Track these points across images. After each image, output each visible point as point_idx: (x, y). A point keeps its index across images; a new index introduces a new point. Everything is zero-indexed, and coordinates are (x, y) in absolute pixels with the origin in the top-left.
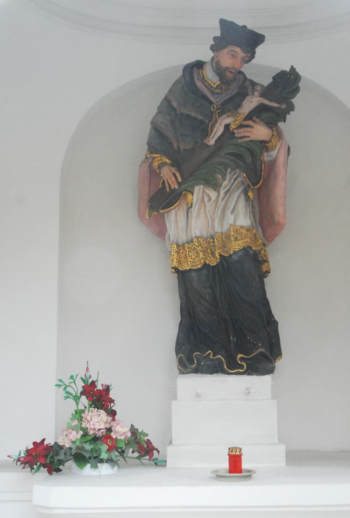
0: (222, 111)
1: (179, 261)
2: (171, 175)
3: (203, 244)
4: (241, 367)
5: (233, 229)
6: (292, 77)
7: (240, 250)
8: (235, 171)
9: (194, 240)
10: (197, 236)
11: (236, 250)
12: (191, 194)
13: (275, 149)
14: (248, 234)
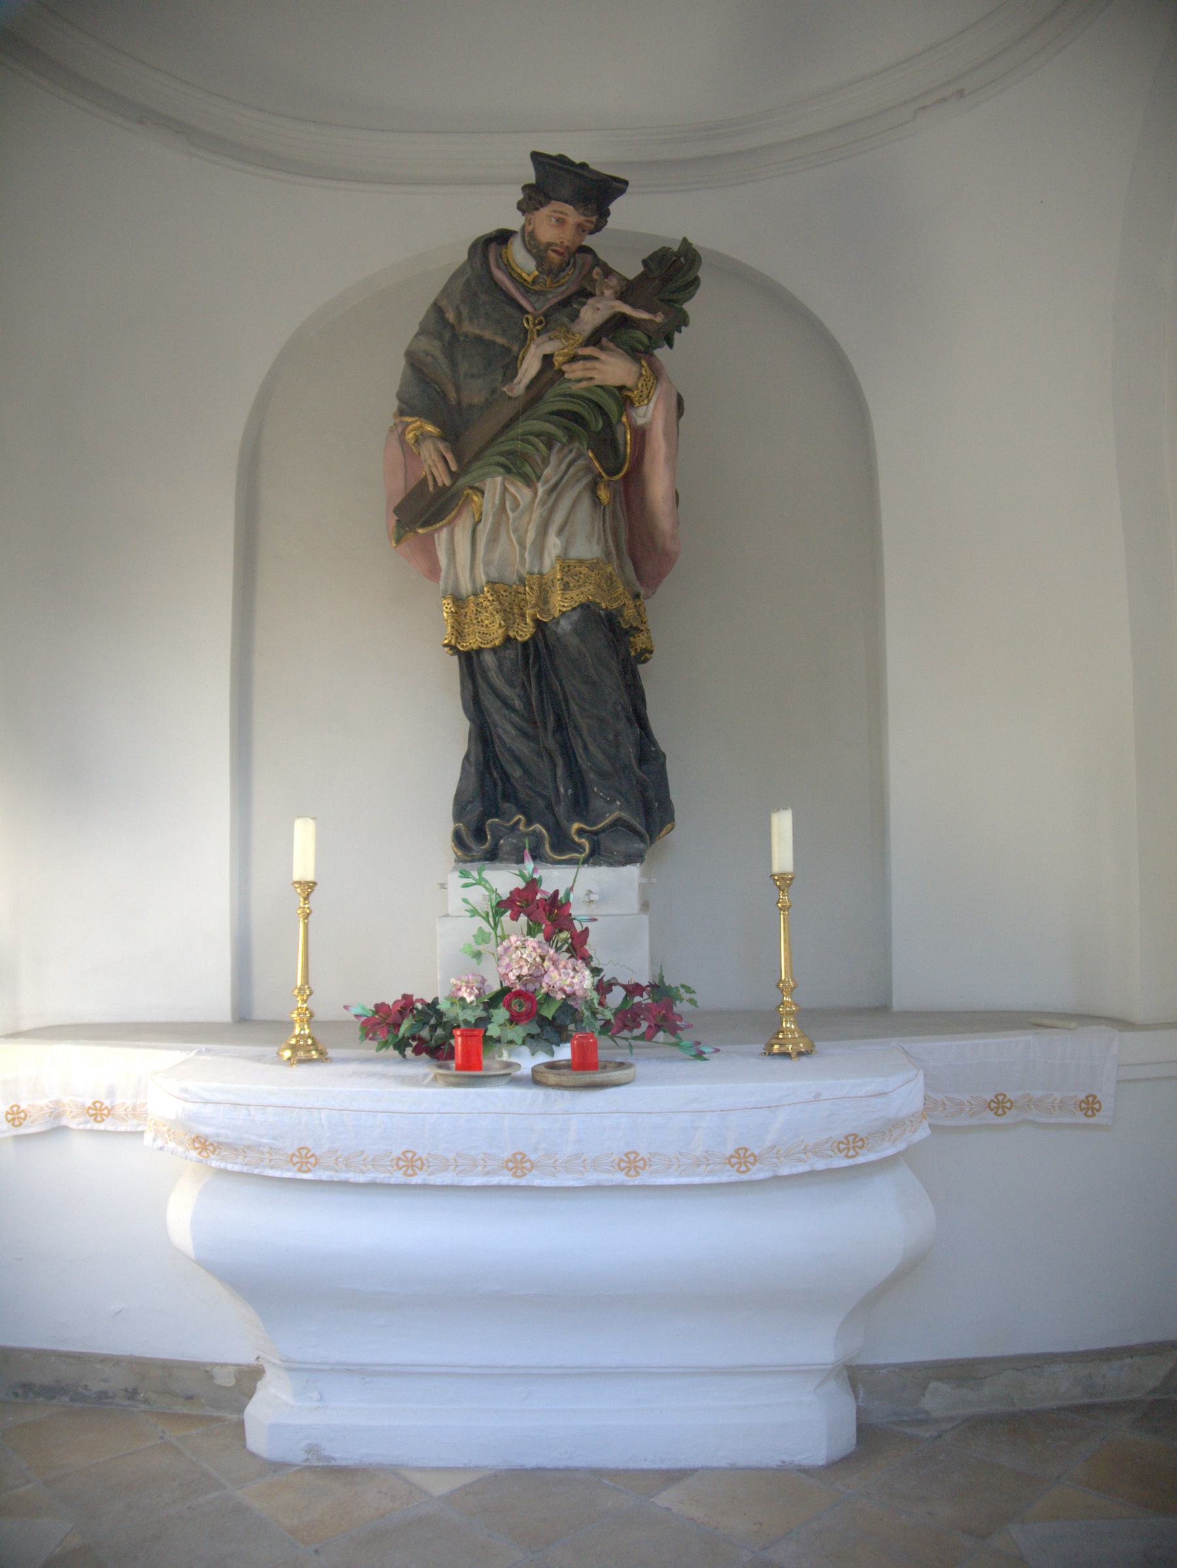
0: (546, 325)
1: (459, 631)
2: (435, 457)
3: (504, 595)
4: (578, 848)
5: (561, 566)
6: (682, 259)
7: (574, 609)
8: (571, 447)
9: (485, 589)
10: (491, 580)
11: (564, 609)
12: (479, 494)
13: (649, 402)
14: (591, 576)
